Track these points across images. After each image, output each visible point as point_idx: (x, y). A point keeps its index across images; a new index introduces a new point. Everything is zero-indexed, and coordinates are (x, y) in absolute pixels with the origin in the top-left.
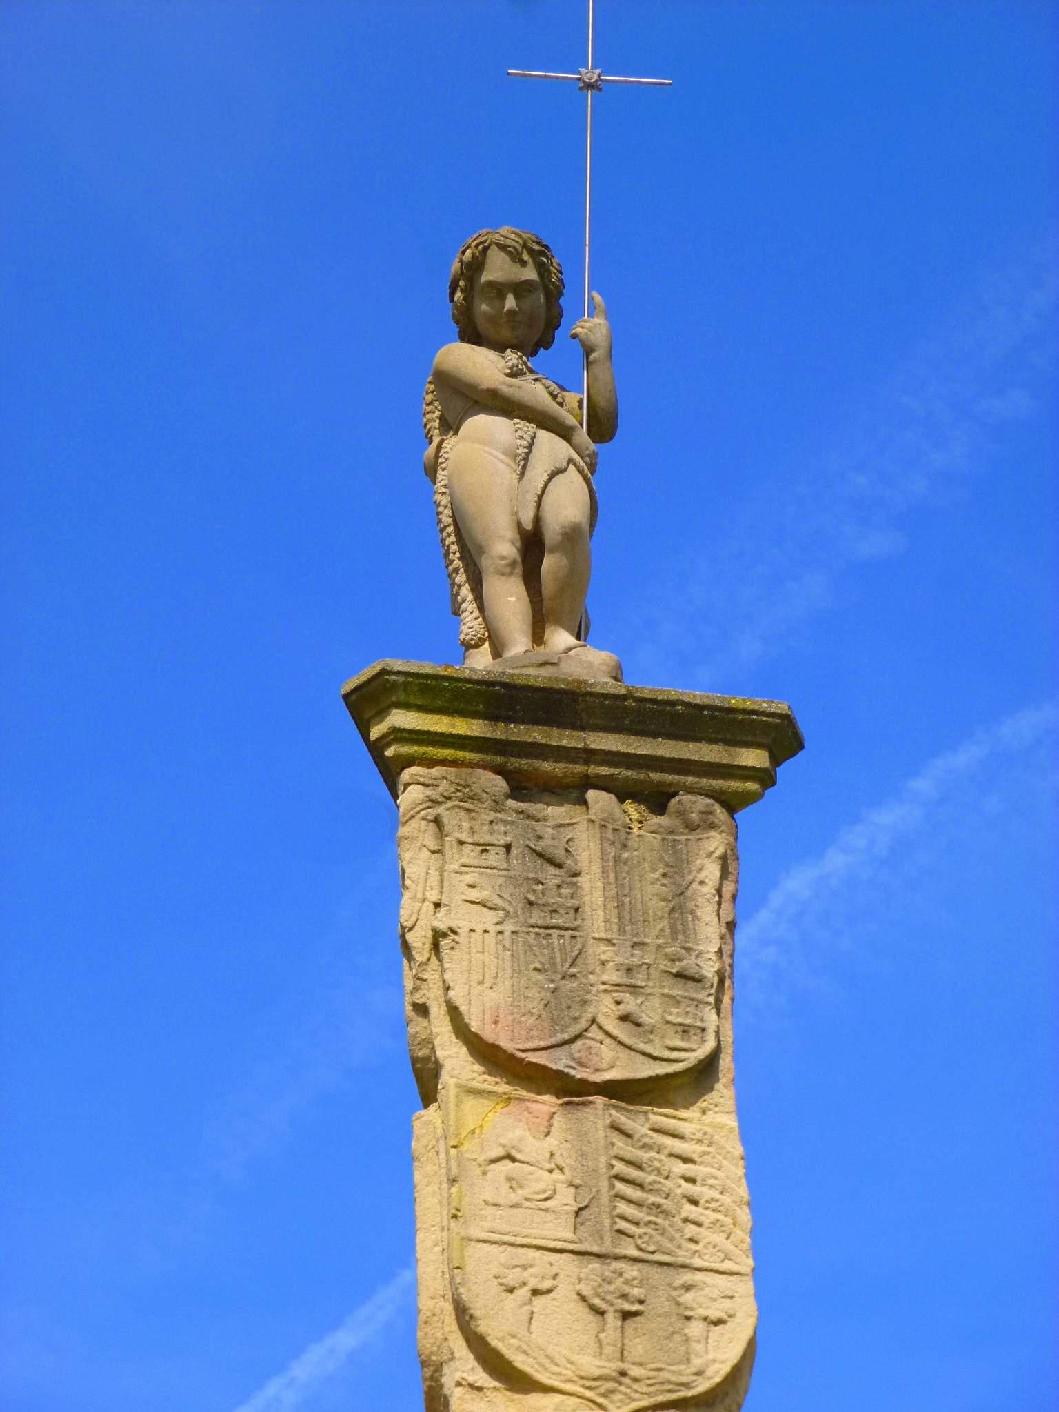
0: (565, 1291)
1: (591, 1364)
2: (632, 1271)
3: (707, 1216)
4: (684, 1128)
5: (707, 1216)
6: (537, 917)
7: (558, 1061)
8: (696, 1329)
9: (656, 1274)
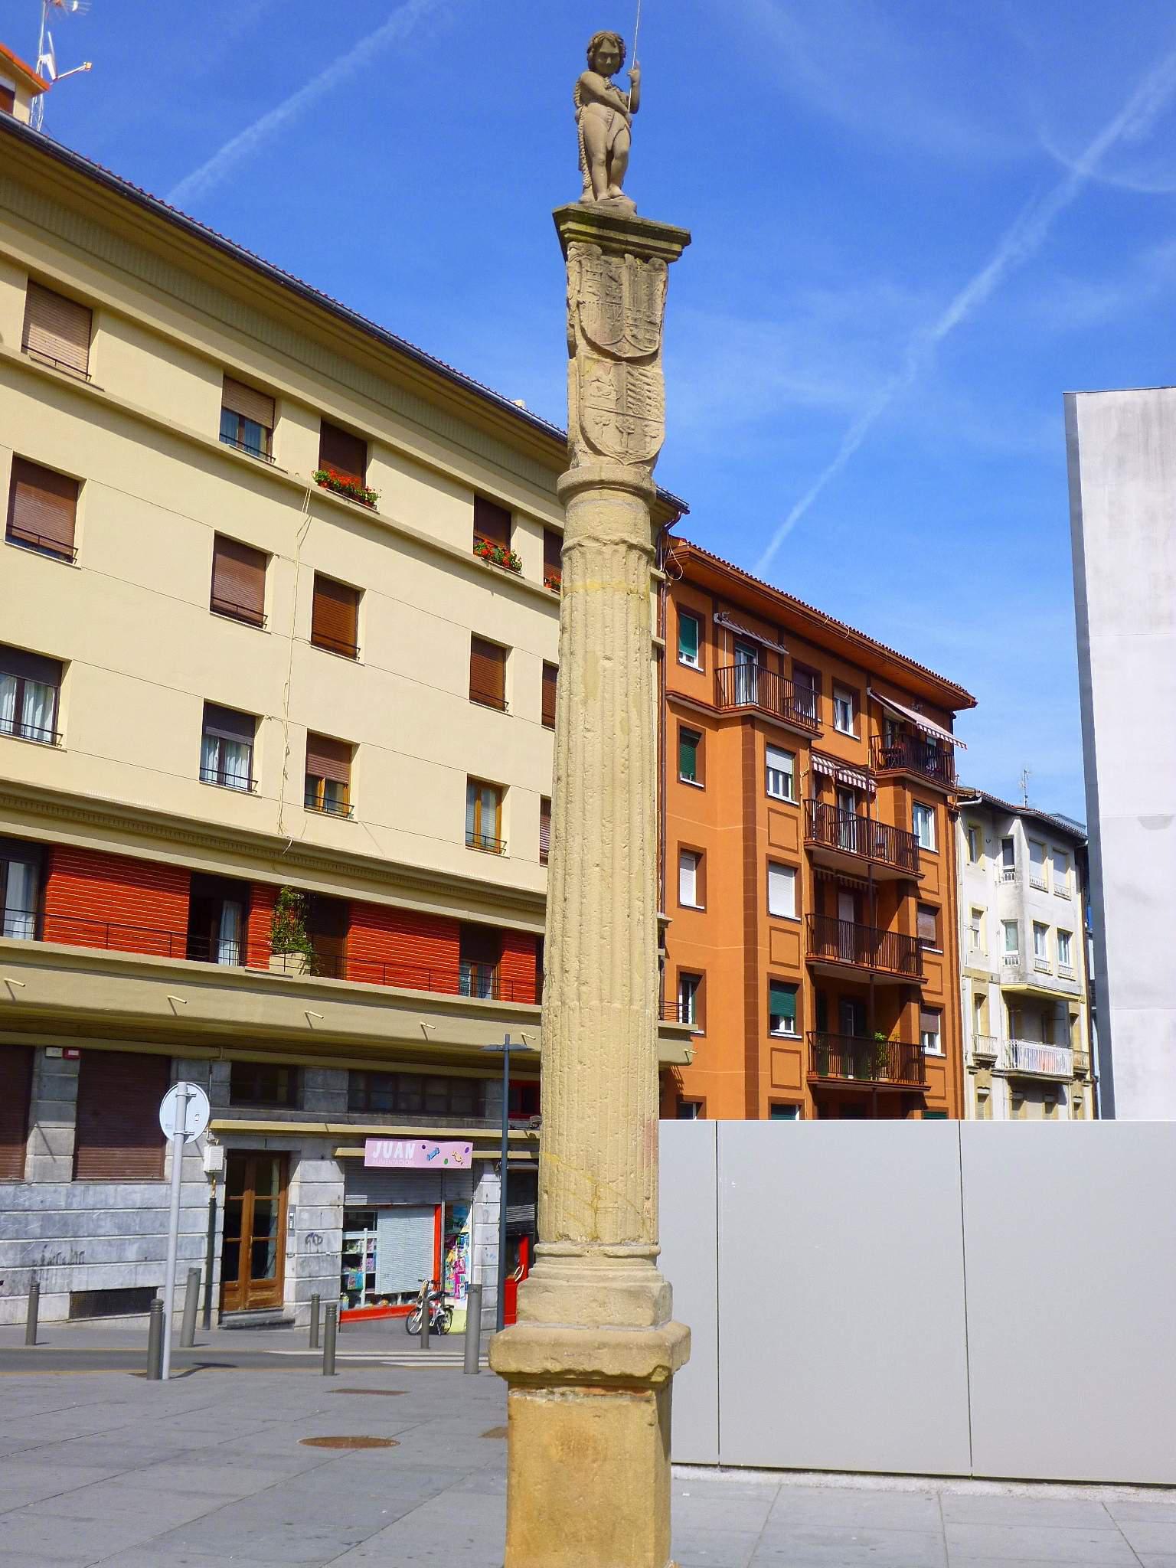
1: (618, 449)
2: (631, 420)
7: (613, 349)
8: (648, 439)
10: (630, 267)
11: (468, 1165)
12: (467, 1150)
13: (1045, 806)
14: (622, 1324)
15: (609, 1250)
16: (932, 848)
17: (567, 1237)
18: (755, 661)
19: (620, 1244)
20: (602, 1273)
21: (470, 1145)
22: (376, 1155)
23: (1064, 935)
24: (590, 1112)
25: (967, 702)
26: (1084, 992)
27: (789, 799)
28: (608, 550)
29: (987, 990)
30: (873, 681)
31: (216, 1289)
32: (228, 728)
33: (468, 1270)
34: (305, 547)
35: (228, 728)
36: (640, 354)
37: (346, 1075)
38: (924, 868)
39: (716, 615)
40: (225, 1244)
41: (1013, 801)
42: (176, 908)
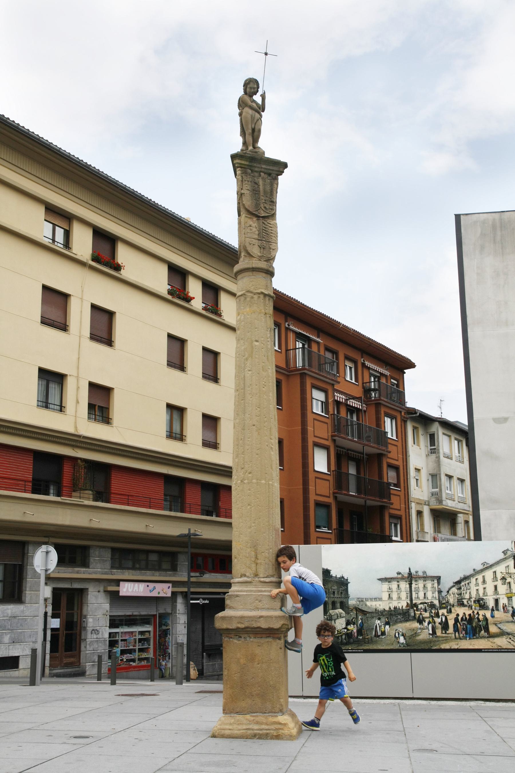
0: (257, 244)
1: (259, 254)
2: (264, 242)
3: (273, 235)
4: (271, 223)
5: (273, 235)
6: (254, 192)
7: (256, 213)
8: (271, 250)
9: (267, 243)
10: (263, 178)
11: (169, 595)
12: (169, 587)
13: (451, 418)
14: (268, 609)
15: (262, 579)
16: (394, 438)
17: (245, 576)
18: (306, 346)
19: (266, 577)
20: (260, 589)
21: (170, 585)
22: (125, 590)
23: (462, 481)
24: (253, 525)
25: (412, 365)
26: (471, 509)
27: (323, 414)
28: (256, 297)
29: (423, 508)
30: (364, 355)
31: (48, 657)
32: (51, 379)
33: (170, 648)
34: (87, 290)
35: (51, 379)
36: (267, 215)
37: (110, 550)
38: (390, 448)
39: (287, 323)
40: (52, 635)
41: (434, 413)
42: (26, 470)
